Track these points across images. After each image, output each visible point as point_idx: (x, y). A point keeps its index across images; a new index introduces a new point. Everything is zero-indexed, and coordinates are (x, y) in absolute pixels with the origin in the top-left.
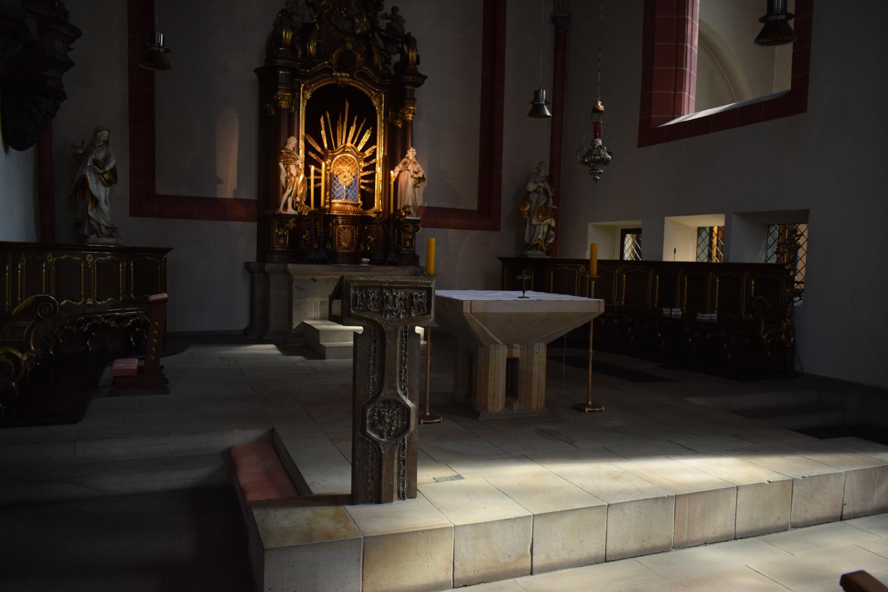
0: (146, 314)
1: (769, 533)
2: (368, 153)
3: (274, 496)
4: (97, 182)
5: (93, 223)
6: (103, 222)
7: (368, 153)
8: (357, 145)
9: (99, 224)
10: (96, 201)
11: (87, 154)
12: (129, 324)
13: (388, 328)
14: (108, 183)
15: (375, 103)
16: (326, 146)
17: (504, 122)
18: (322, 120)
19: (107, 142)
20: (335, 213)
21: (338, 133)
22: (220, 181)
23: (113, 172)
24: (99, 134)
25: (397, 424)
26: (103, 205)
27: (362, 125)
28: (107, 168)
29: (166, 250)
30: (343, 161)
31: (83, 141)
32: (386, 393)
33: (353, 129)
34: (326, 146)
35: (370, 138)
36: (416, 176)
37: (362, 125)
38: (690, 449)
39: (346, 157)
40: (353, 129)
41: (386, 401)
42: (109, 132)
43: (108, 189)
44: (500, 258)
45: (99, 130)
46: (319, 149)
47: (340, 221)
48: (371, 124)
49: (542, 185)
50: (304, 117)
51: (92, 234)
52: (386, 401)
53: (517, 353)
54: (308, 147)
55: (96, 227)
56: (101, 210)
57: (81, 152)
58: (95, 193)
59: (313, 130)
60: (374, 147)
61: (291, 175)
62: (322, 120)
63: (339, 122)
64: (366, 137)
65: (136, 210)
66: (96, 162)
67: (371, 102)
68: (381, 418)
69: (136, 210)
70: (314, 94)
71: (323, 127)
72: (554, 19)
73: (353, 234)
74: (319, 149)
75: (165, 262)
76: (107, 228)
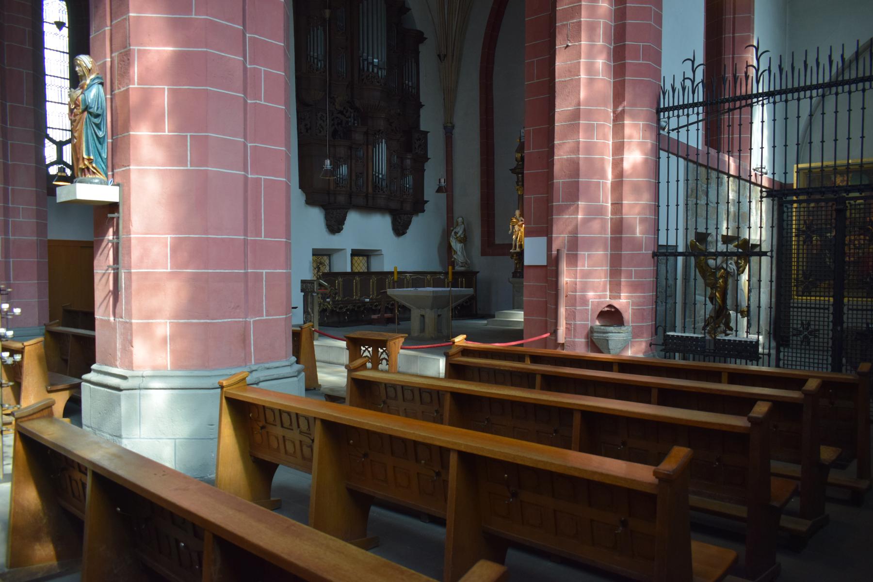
10: (456, 252)
14: (460, 242)
26: (459, 253)
42: (463, 219)
56: (458, 255)
65: (484, 253)
76: (462, 263)
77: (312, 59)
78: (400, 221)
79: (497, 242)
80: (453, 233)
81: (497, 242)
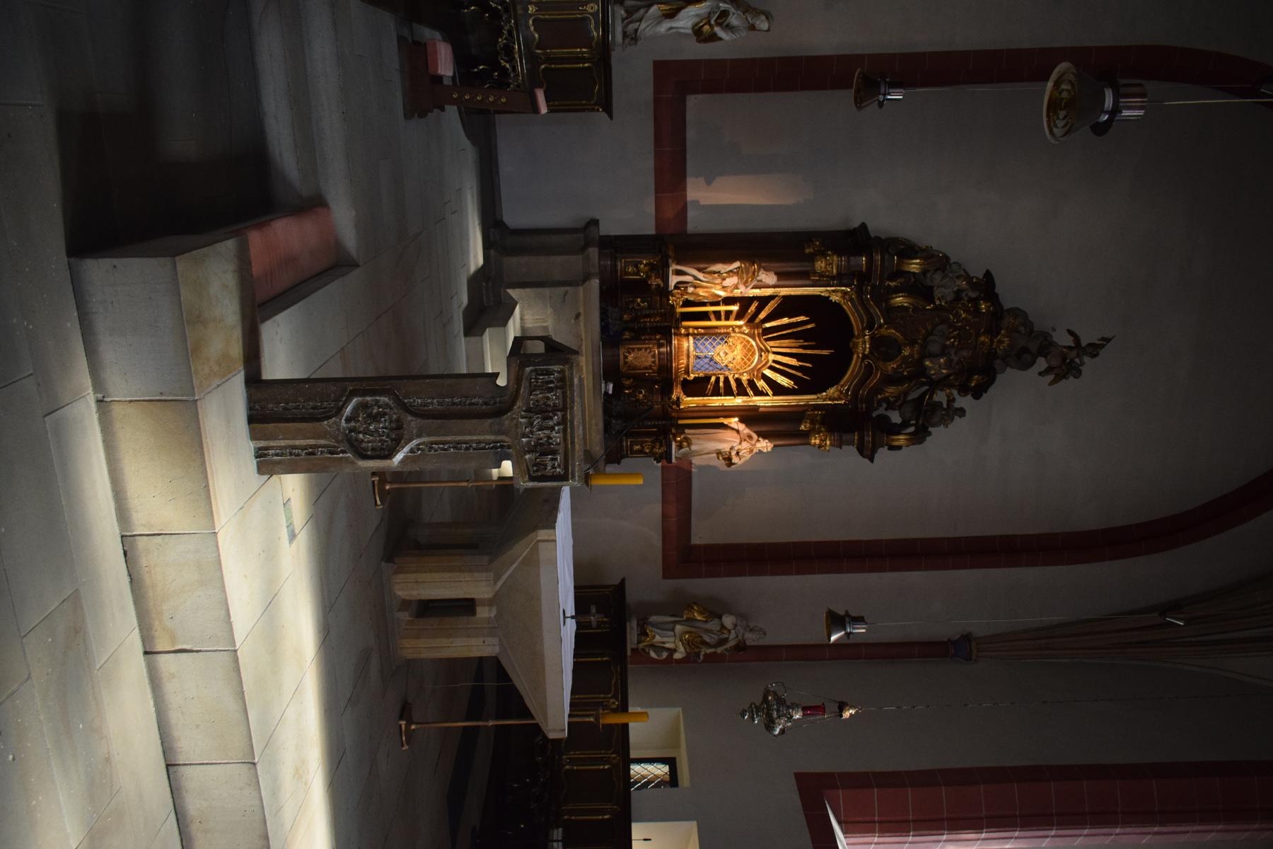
0: (518, 86)
2: (761, 384)
4: (697, 15)
5: (642, 11)
6: (643, 25)
7: (761, 384)
9: (640, 20)
10: (671, 15)
12: (503, 63)
13: (506, 420)
14: (697, 31)
15: (831, 391)
16: (768, 325)
18: (802, 318)
19: (752, 28)
20: (675, 342)
21: (786, 342)
22: (709, 183)
23: (713, 38)
24: (763, 17)
25: (367, 441)
26: (666, 25)
27: (799, 374)
28: (717, 29)
29: (608, 110)
30: (749, 351)
32: (412, 423)
33: (793, 362)
34: (768, 325)
35: (782, 387)
36: (733, 453)
37: (799, 374)
39: (753, 354)
40: (793, 362)
42: (768, 30)
43: (690, 31)
44: (623, 581)
45: (768, 16)
46: (762, 315)
47: (663, 350)
48: (802, 387)
49: (733, 635)
51: (626, 11)
53: (483, 613)
54: (763, 301)
55: (636, 16)
56: (659, 23)
58: (683, 13)
59: (788, 306)
60: (770, 392)
61: (724, 279)
62: (802, 318)
63: (801, 342)
64: (783, 381)
65: (663, 70)
66: (725, 14)
68: (375, 418)
69: (663, 70)
70: (837, 305)
71: (794, 320)
73: (646, 368)
74: (762, 315)
75: (593, 110)
76: (636, 30)
79: (692, 101)
81: (692, 101)
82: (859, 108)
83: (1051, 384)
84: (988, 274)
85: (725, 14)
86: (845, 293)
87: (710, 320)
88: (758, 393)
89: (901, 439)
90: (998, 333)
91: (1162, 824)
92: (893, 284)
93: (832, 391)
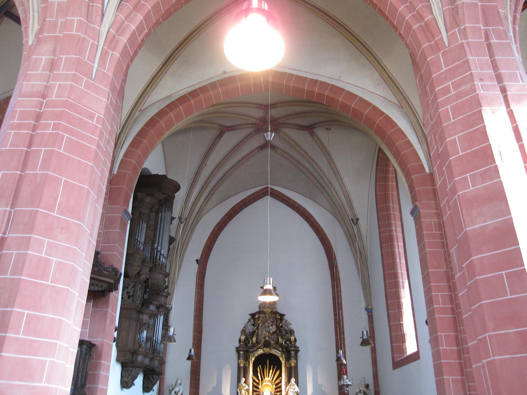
1: (381, 248)
2: (278, 381)
3: (173, 95)
7: (278, 381)
8: (272, 380)
11: (173, 389)
17: (293, 198)
19: (180, 384)
21: (265, 374)
31: (172, 385)
33: (271, 371)
35: (280, 373)
38: (289, 68)
41: (256, 345)
45: (177, 380)
46: (257, 381)
49: (362, 389)
50: (252, 369)
52: (256, 345)
54: (254, 381)
57: (171, 388)
59: (255, 373)
60: (280, 378)
63: (265, 369)
64: (278, 373)
67: (279, 359)
72: (366, 309)
74: (257, 381)
77: (138, 243)
78: (152, 379)
80: (173, 392)
82: (122, 389)
83: (146, 388)
84: (250, 315)
85: (175, 392)
86: (252, 356)
87: (71, 321)
88: (281, 382)
89: (292, 338)
90: (265, 312)
91: (395, 259)
92: (251, 342)
93: (281, 359)
